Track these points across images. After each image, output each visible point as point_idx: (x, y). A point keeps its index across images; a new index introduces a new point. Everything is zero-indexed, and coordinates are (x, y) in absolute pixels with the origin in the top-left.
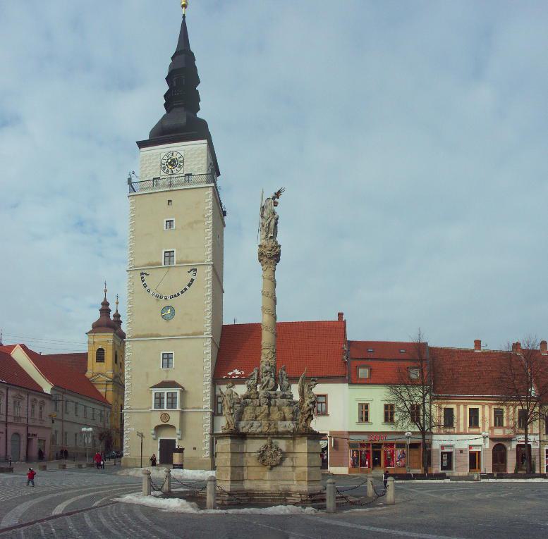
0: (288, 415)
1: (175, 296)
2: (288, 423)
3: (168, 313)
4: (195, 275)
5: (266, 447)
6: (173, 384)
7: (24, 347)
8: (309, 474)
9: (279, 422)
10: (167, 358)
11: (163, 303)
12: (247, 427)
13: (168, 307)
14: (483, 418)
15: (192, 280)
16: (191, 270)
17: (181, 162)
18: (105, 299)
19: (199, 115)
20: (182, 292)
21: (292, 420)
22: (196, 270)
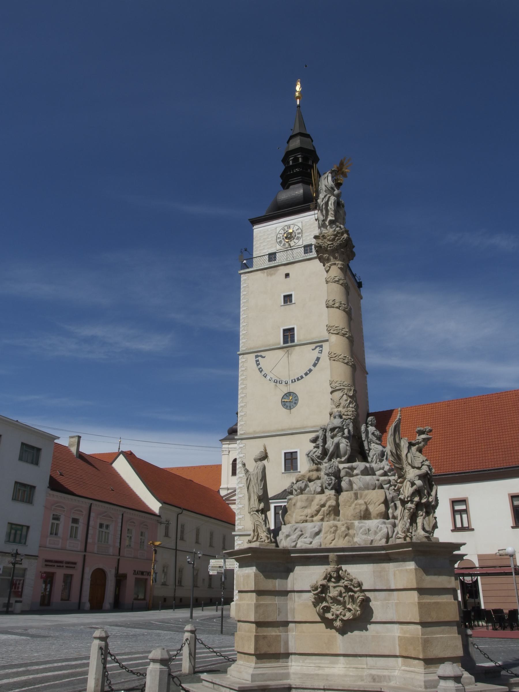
0: (377, 508)
1: (298, 379)
2: (373, 523)
5: (328, 577)
7: (130, 457)
8: (426, 643)
9: (356, 523)
12: (294, 537)
15: (318, 359)
16: (316, 347)
17: (299, 233)
21: (385, 516)
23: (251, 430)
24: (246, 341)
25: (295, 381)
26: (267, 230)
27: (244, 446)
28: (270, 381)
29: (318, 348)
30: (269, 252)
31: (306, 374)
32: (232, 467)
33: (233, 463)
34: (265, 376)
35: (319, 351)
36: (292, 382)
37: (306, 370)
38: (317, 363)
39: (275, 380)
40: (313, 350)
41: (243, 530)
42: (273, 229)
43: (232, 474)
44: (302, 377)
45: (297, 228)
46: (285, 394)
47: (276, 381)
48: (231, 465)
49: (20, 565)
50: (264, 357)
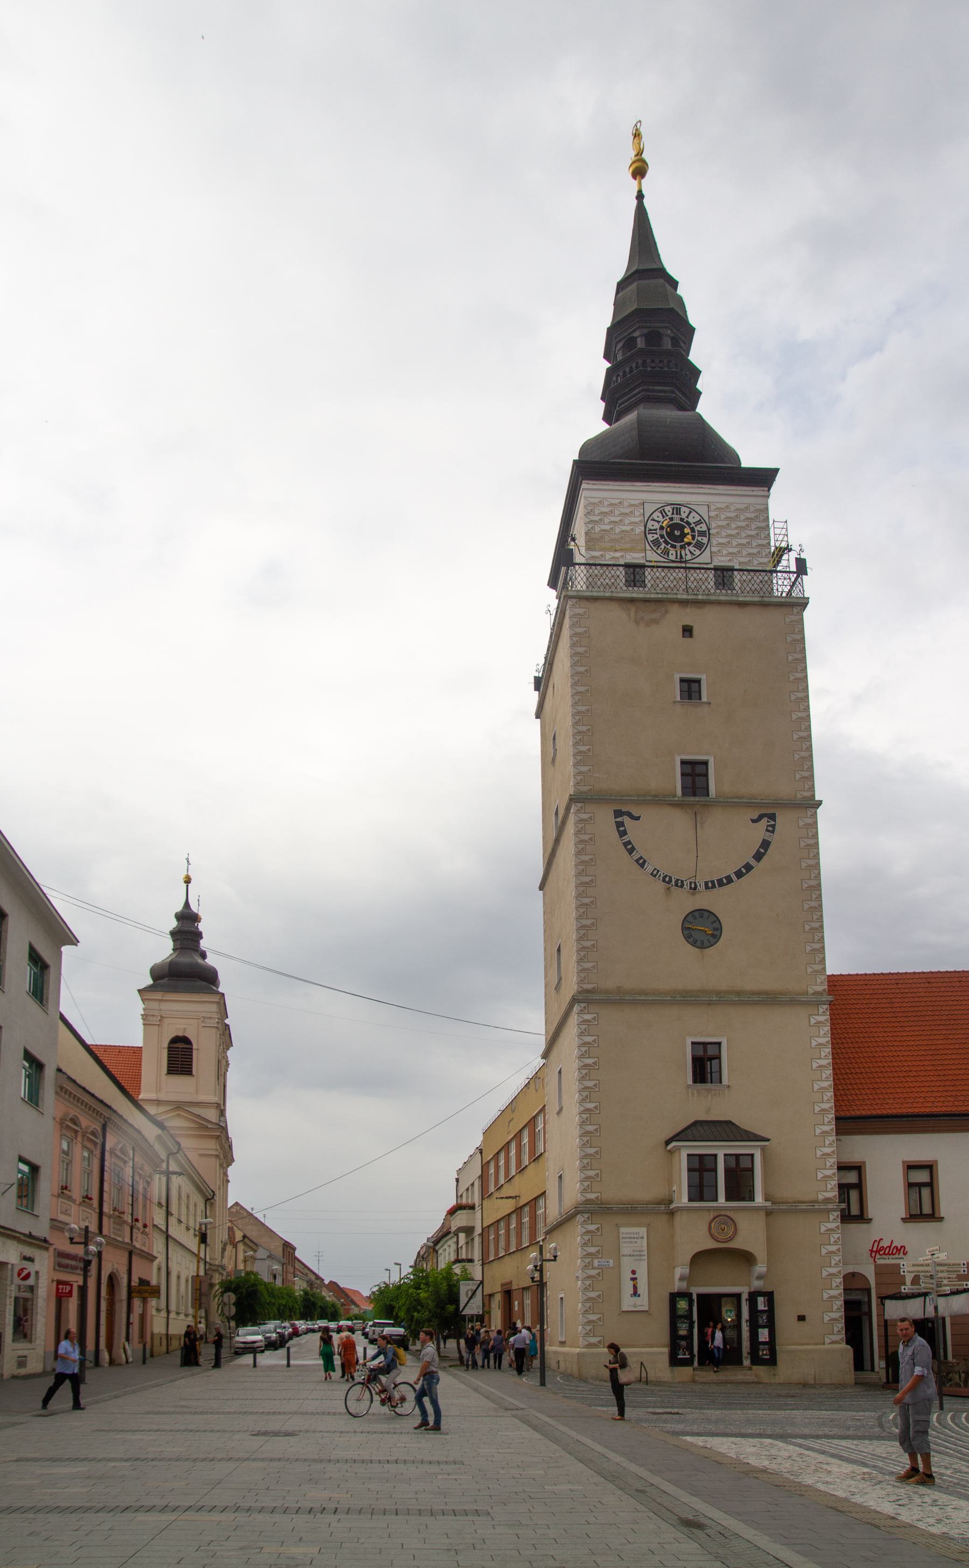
4: (772, 829)
11: (686, 903)
13: (701, 912)
15: (766, 844)
18: (187, 904)
19: (608, 365)
22: (772, 817)
23: (610, 984)
24: (589, 771)
25: (714, 886)
26: (620, 503)
27: (594, 1019)
28: (655, 876)
29: (766, 819)
30: (627, 561)
31: (739, 874)
32: (169, 1054)
33: (171, 1046)
34: (641, 863)
35: (768, 826)
36: (707, 887)
37: (739, 865)
38: (764, 854)
39: (666, 876)
40: (754, 821)
41: (599, 1202)
42: (636, 502)
43: (168, 1070)
44: (729, 880)
45: (698, 518)
46: (691, 912)
47: (667, 879)
48: (166, 1051)
49: (40, 1275)
50: (638, 818)
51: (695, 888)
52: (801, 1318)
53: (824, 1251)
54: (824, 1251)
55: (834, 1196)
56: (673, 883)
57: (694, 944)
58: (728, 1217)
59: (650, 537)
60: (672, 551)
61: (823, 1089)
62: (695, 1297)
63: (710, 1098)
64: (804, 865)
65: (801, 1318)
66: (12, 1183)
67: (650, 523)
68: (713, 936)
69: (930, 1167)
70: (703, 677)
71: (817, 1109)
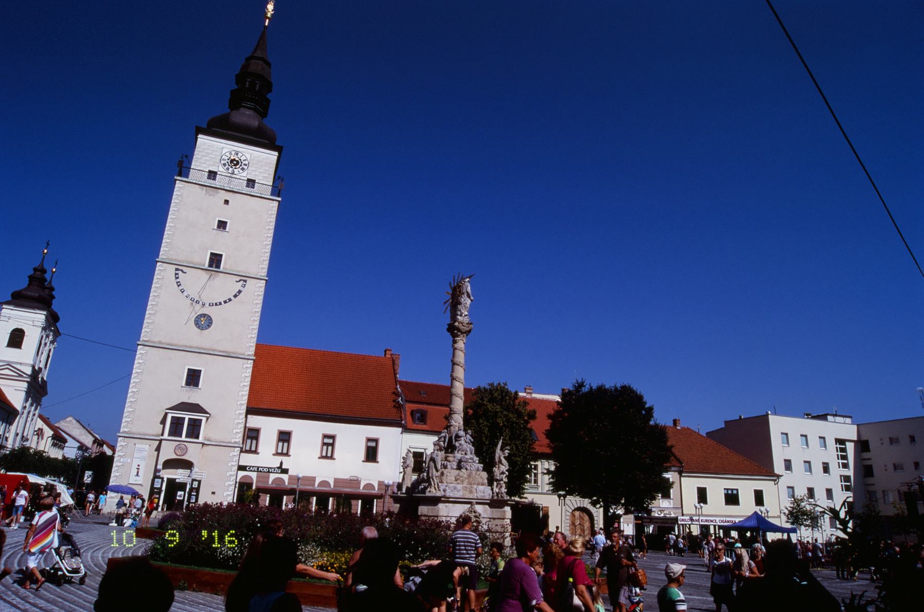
1: (216, 304)
3: (204, 322)
6: (196, 408)
10: (193, 378)
13: (204, 315)
14: (693, 560)
15: (240, 292)
16: (240, 280)
20: (225, 302)
22: (245, 281)
25: (213, 305)
29: (242, 281)
36: (210, 305)
37: (226, 298)
45: (245, 158)
47: (192, 299)
50: (185, 273)
51: (204, 305)
52: (213, 493)
53: (229, 465)
54: (229, 465)
55: (239, 441)
56: (195, 301)
57: (199, 327)
58: (185, 445)
59: (222, 162)
60: (231, 169)
61: (243, 395)
62: (165, 480)
63: (191, 393)
64: (255, 302)
65: (213, 493)
66: (802, 449)
67: (223, 157)
68: (208, 326)
69: (333, 437)
70: (229, 222)
71: (239, 403)
